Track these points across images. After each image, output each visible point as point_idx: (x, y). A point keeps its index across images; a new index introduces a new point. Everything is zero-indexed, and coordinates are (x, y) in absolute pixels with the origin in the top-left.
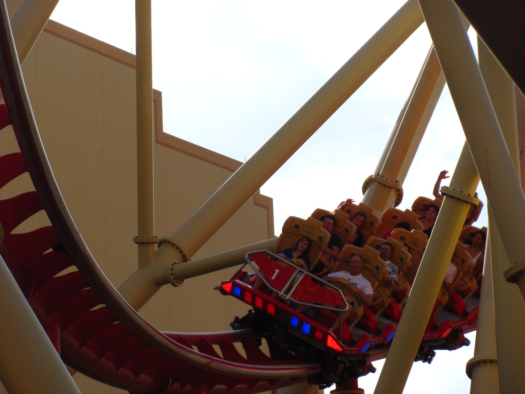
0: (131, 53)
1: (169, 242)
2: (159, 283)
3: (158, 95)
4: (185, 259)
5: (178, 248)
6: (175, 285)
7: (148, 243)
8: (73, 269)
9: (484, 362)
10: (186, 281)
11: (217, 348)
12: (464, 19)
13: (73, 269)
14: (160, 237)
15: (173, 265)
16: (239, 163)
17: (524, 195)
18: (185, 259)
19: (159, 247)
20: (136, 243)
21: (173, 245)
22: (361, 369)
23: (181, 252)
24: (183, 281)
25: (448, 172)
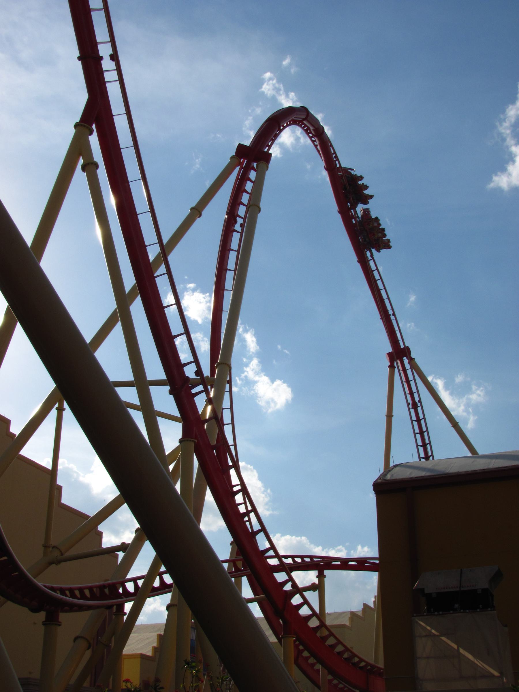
0: (348, 621)
1: (56, 547)
2: (50, 563)
3: (60, 488)
4: (62, 555)
5: (60, 550)
6: (56, 565)
7: (47, 547)
8: (5, 558)
9: (88, 164)
10: (62, 564)
11: (67, 592)
12: (180, 496)
13: (5, 558)
14: (53, 545)
15: (57, 556)
16: (89, 517)
17: (1, 527)
18: (62, 555)
19: (52, 549)
20: (43, 546)
21: (58, 548)
22: (348, 205)
23: (61, 551)
24: (60, 563)
25: (387, 245)
